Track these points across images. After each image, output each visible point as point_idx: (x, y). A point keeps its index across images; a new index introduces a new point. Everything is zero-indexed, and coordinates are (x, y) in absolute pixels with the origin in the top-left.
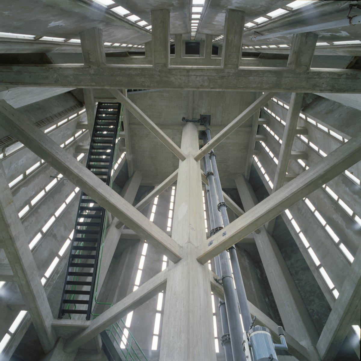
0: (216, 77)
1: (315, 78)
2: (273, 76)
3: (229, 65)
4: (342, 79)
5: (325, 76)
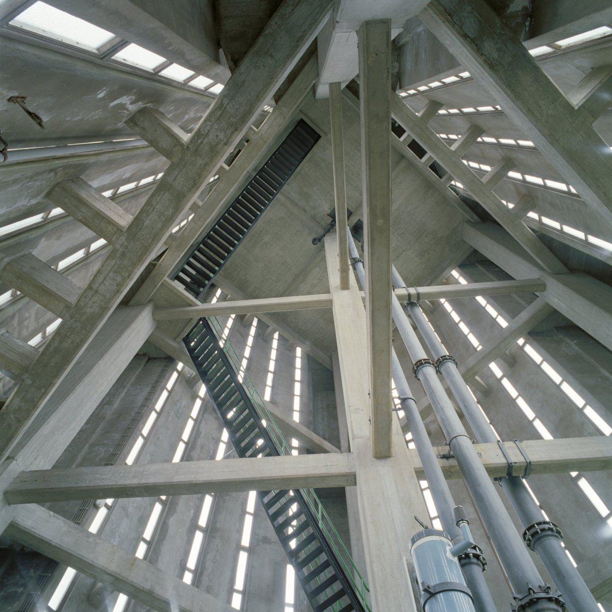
0: (118, 262)
1: (202, 143)
2: (161, 195)
3: (113, 240)
4: (227, 107)
5: (208, 128)
